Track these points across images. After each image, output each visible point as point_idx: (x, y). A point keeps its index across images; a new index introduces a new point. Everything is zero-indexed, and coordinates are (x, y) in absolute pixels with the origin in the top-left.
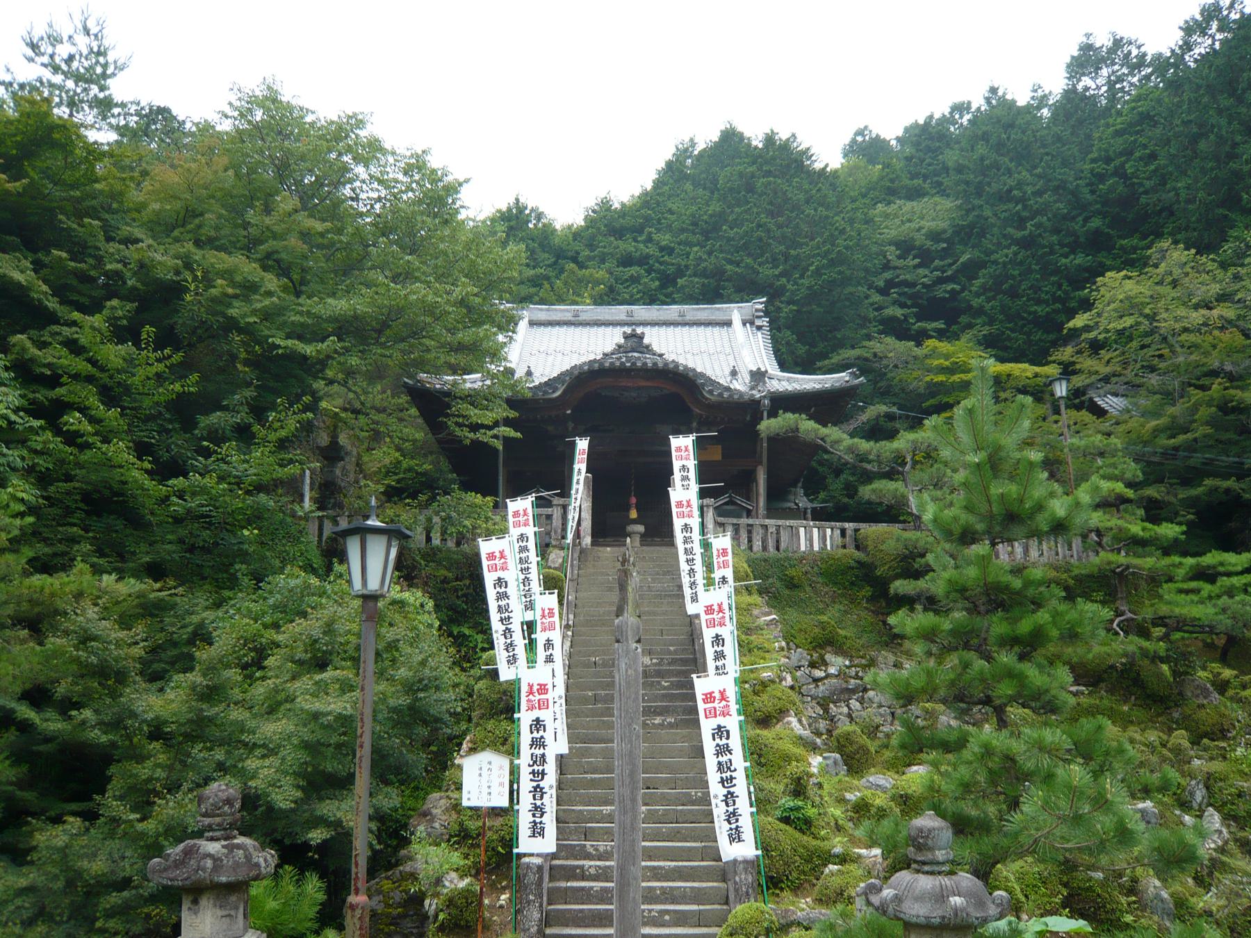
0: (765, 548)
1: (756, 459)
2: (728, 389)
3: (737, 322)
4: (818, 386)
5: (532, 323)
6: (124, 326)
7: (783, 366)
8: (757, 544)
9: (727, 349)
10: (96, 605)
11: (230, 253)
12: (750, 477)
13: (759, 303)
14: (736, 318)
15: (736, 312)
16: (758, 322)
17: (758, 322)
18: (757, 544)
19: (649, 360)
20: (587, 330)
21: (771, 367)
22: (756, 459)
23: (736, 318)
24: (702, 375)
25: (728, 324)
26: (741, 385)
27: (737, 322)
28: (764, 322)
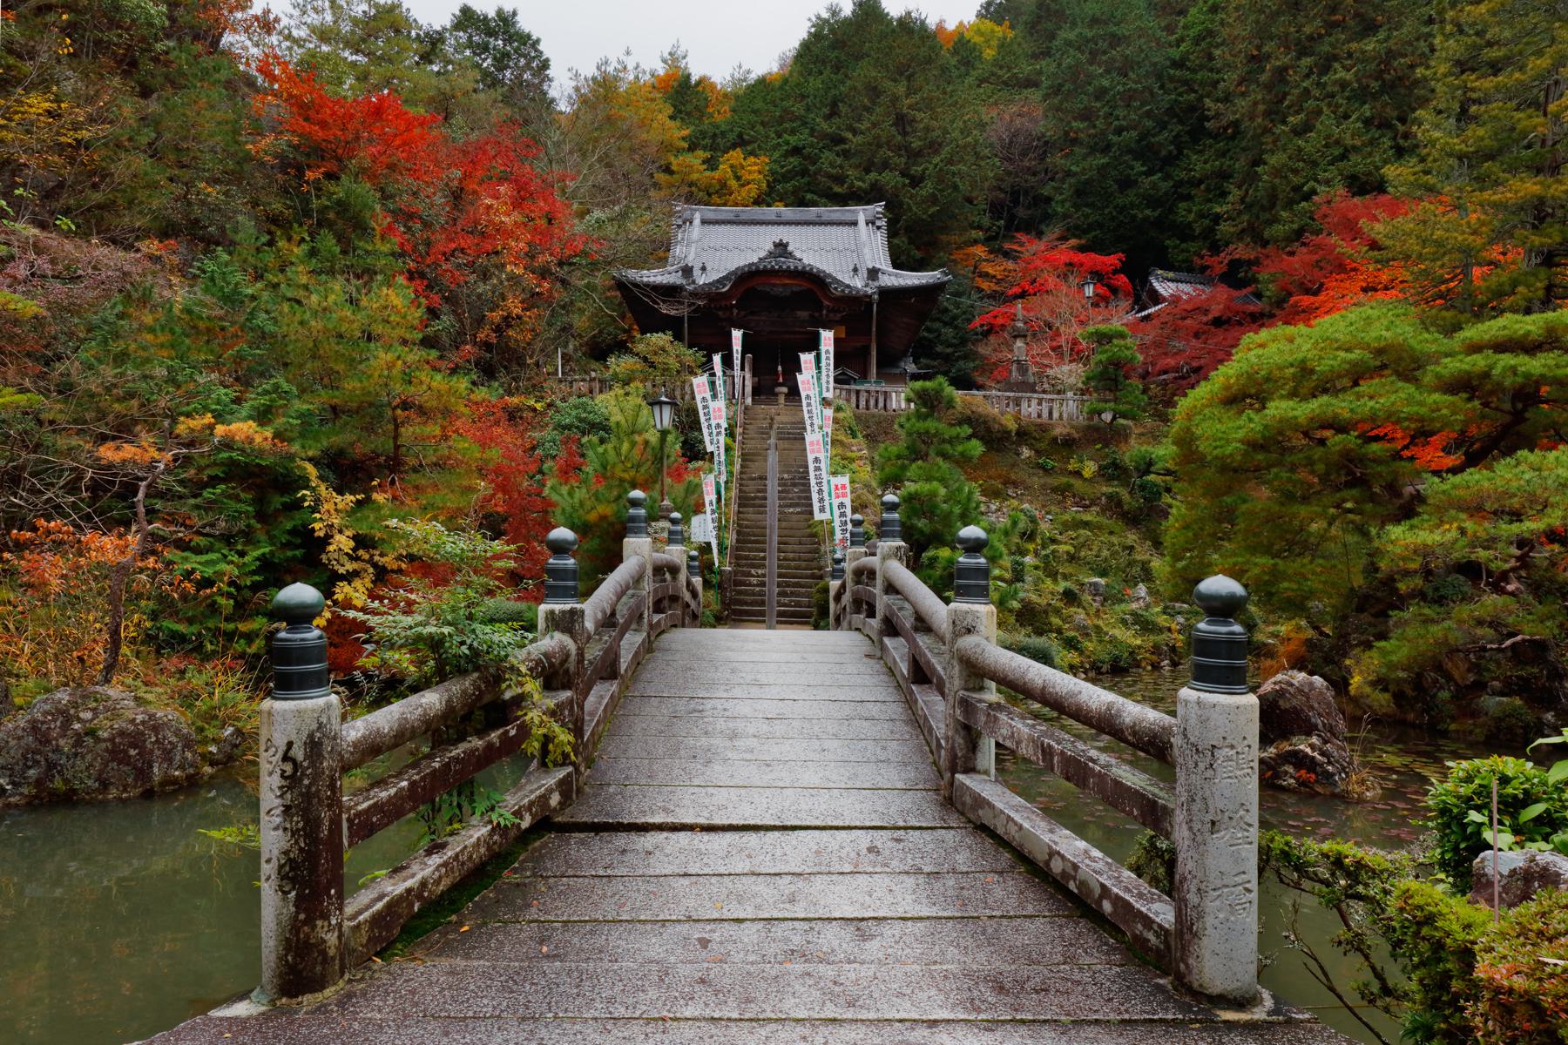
0: (868, 408)
1: (881, 334)
2: (848, 286)
3: (862, 223)
4: (916, 282)
5: (704, 222)
6: (1186, 269)
7: (895, 266)
8: (862, 403)
9: (849, 249)
10: (154, 616)
11: (769, 205)
12: (866, 351)
13: (879, 207)
14: (861, 219)
15: (862, 213)
16: (878, 223)
17: (878, 223)
18: (862, 403)
19: (791, 264)
20: (746, 228)
21: (884, 263)
22: (881, 334)
23: (861, 219)
24: (830, 275)
25: (855, 224)
26: (858, 283)
27: (862, 223)
28: (883, 223)
